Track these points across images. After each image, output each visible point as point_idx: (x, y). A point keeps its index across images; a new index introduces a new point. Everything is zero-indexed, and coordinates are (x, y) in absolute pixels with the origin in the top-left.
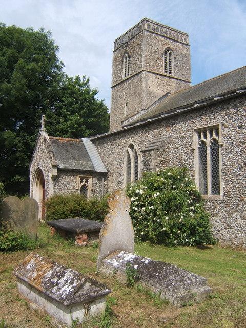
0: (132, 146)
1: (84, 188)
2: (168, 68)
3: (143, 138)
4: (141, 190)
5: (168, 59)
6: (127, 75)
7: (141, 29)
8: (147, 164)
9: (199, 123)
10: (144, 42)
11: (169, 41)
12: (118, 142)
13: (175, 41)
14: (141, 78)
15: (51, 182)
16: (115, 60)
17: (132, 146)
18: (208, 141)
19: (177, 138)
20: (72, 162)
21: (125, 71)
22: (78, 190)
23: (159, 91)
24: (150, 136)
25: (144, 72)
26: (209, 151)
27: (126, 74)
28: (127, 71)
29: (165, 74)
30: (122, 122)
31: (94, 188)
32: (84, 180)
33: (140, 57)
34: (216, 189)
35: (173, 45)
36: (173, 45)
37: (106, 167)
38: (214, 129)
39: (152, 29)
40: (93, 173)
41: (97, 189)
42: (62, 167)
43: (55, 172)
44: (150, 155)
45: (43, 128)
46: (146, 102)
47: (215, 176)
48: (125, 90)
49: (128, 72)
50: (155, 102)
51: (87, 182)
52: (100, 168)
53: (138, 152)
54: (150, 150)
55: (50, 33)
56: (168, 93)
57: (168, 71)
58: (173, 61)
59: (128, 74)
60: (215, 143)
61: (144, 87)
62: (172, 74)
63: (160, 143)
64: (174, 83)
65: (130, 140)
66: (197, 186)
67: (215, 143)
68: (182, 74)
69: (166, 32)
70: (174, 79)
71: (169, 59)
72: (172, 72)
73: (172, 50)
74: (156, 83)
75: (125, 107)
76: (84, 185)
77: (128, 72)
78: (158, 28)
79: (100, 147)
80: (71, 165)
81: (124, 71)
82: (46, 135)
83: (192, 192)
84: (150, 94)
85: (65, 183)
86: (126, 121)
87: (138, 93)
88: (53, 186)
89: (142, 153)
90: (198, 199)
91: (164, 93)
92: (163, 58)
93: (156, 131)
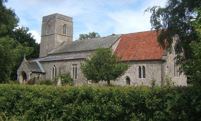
0: (55, 66)
2: (64, 32)
4: (189, 31)
8: (60, 72)
9: (73, 63)
11: (65, 21)
12: (50, 64)
13: (68, 21)
15: (29, 75)
16: (43, 25)
17: (55, 66)
18: (75, 67)
23: (61, 41)
26: (75, 69)
30: (47, 53)
34: (76, 78)
35: (66, 23)
36: (66, 23)
37: (45, 71)
38: (76, 65)
40: (41, 73)
43: (31, 73)
45: (25, 58)
46: (56, 45)
47: (76, 75)
48: (47, 39)
52: (43, 71)
53: (57, 68)
55: (14, 10)
60: (76, 68)
64: (67, 38)
66: (72, 77)
67: (76, 68)
80: (35, 70)
81: (47, 31)
82: (26, 60)
83: (71, 79)
84: (58, 43)
87: (53, 42)
90: (72, 80)
91: (63, 42)
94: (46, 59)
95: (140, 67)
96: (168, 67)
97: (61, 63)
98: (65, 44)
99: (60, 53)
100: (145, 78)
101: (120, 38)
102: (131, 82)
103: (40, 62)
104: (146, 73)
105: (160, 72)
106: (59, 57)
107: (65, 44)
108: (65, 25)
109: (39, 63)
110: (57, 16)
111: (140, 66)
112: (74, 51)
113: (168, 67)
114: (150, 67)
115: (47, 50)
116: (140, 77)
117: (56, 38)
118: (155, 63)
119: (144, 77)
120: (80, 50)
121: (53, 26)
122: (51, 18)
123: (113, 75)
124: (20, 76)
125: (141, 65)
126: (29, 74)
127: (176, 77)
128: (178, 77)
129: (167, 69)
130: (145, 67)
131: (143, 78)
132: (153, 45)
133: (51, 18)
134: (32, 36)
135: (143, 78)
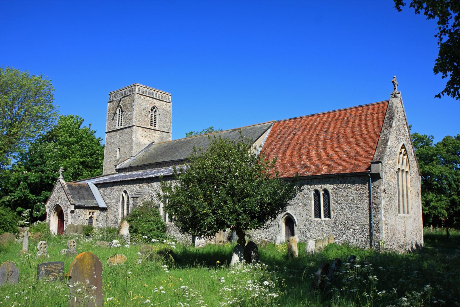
0: (125, 192)
1: (91, 218)
2: (153, 122)
3: (133, 188)
5: (153, 116)
6: (120, 125)
7: (133, 91)
10: (135, 103)
11: (155, 101)
12: (115, 187)
14: (132, 131)
15: (70, 214)
19: (152, 191)
20: (82, 201)
21: (119, 122)
22: (87, 220)
23: (146, 142)
24: (137, 187)
25: (134, 127)
27: (119, 124)
28: (120, 122)
29: (150, 127)
31: (97, 219)
32: (91, 213)
33: (132, 114)
35: (157, 103)
36: (157, 103)
37: (106, 204)
39: (142, 92)
41: (100, 219)
42: (77, 205)
43: (73, 208)
44: (137, 200)
45: (61, 176)
49: (121, 123)
50: (142, 150)
51: (93, 213)
52: (102, 205)
53: (130, 196)
54: (137, 197)
56: (153, 142)
57: (153, 124)
58: (157, 116)
59: (121, 125)
61: (134, 139)
62: (157, 127)
63: (143, 193)
65: (124, 188)
68: (164, 127)
69: (153, 93)
70: (158, 131)
71: (155, 115)
72: (157, 125)
73: (157, 108)
74: (143, 135)
75: (118, 151)
76: (91, 216)
77: (121, 123)
78: (146, 91)
79: (102, 189)
80: (82, 203)
82: (63, 181)
84: (139, 144)
85: (79, 215)
86: (119, 165)
88: (70, 217)
89: (132, 199)
91: (150, 143)
92: (150, 115)
93: (141, 185)
94: (113, 178)
95: (317, 192)
96: (385, 192)
97: (137, 186)
98: (154, 146)
99: (141, 166)
100: (329, 217)
101: (269, 128)
102: (296, 228)
103: (96, 185)
104: (333, 205)
105: (366, 202)
106: (137, 174)
107: (154, 146)
108: (154, 108)
109: (95, 190)
110: (137, 90)
111: (318, 189)
112: (169, 159)
113: (385, 192)
114: (341, 192)
115: (118, 160)
116: (318, 215)
117: (134, 135)
118: (353, 183)
119: (328, 215)
120: (182, 158)
121: (129, 110)
122: (125, 94)
123: (252, 215)
124: (52, 216)
125: (320, 188)
126: (69, 211)
127: (401, 215)
128: (406, 215)
129: (383, 195)
130: (330, 191)
131: (325, 217)
132: (345, 140)
133: (125, 94)
134: (382, 252)
135: (316, 217)
